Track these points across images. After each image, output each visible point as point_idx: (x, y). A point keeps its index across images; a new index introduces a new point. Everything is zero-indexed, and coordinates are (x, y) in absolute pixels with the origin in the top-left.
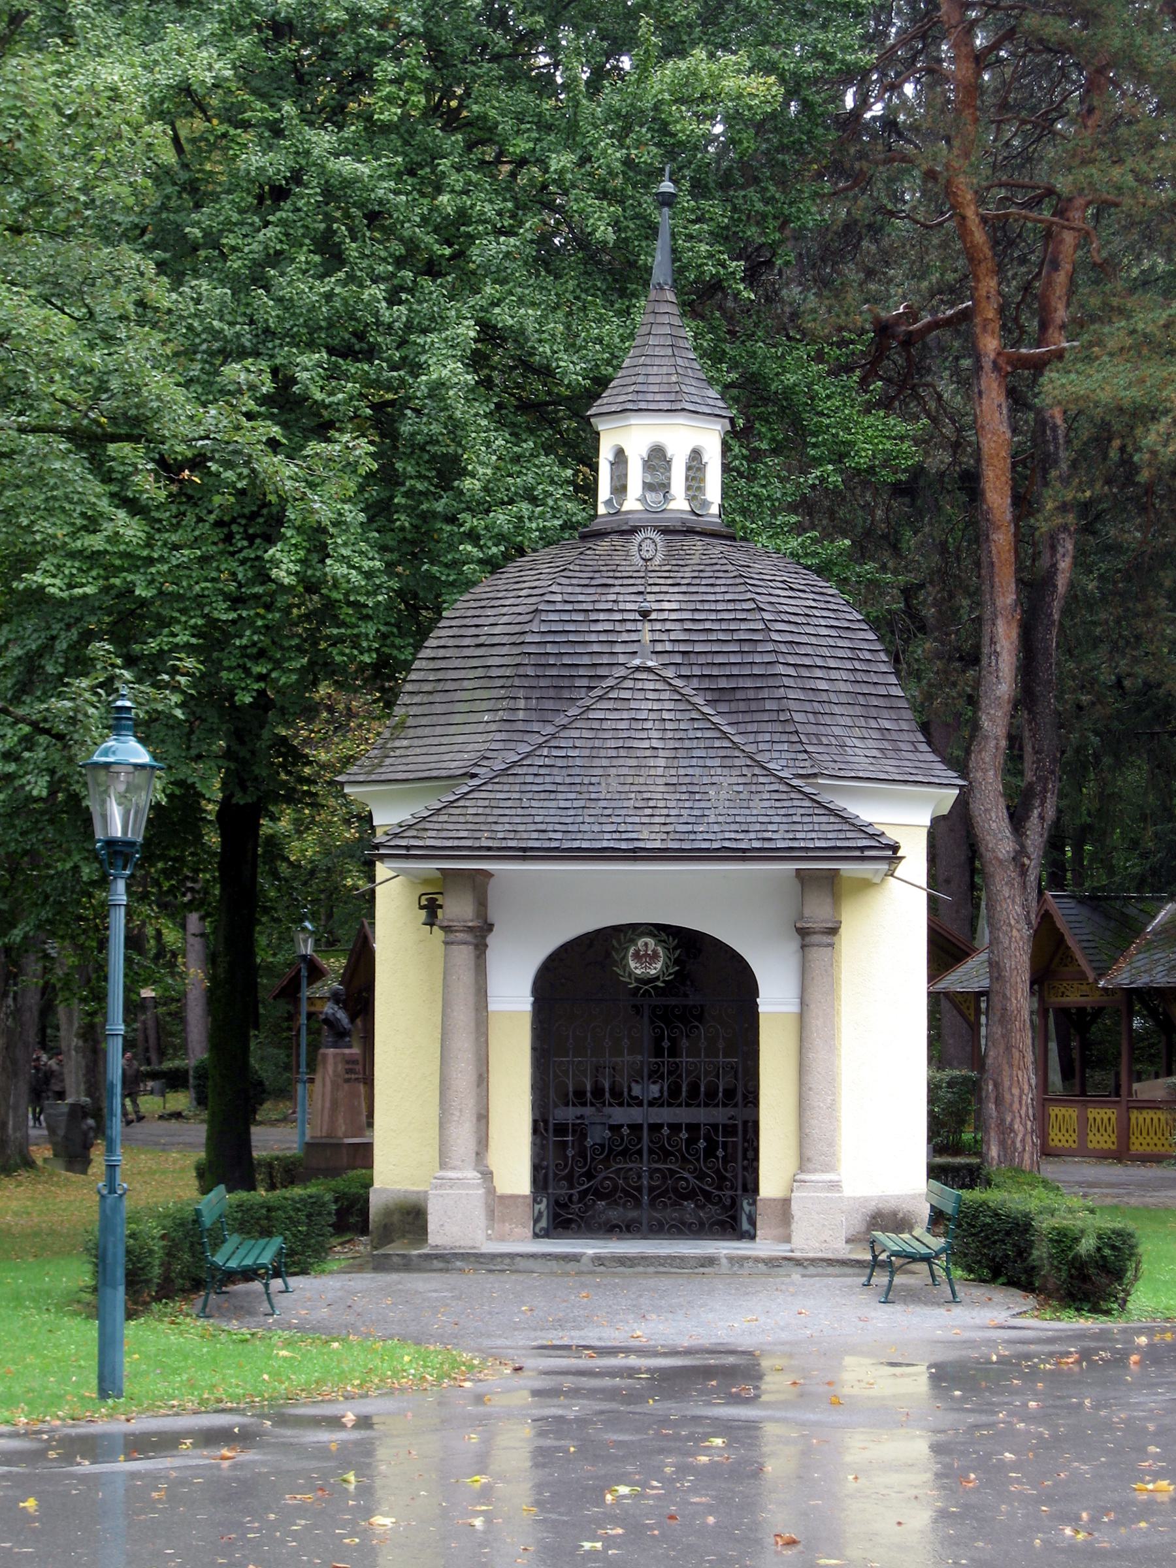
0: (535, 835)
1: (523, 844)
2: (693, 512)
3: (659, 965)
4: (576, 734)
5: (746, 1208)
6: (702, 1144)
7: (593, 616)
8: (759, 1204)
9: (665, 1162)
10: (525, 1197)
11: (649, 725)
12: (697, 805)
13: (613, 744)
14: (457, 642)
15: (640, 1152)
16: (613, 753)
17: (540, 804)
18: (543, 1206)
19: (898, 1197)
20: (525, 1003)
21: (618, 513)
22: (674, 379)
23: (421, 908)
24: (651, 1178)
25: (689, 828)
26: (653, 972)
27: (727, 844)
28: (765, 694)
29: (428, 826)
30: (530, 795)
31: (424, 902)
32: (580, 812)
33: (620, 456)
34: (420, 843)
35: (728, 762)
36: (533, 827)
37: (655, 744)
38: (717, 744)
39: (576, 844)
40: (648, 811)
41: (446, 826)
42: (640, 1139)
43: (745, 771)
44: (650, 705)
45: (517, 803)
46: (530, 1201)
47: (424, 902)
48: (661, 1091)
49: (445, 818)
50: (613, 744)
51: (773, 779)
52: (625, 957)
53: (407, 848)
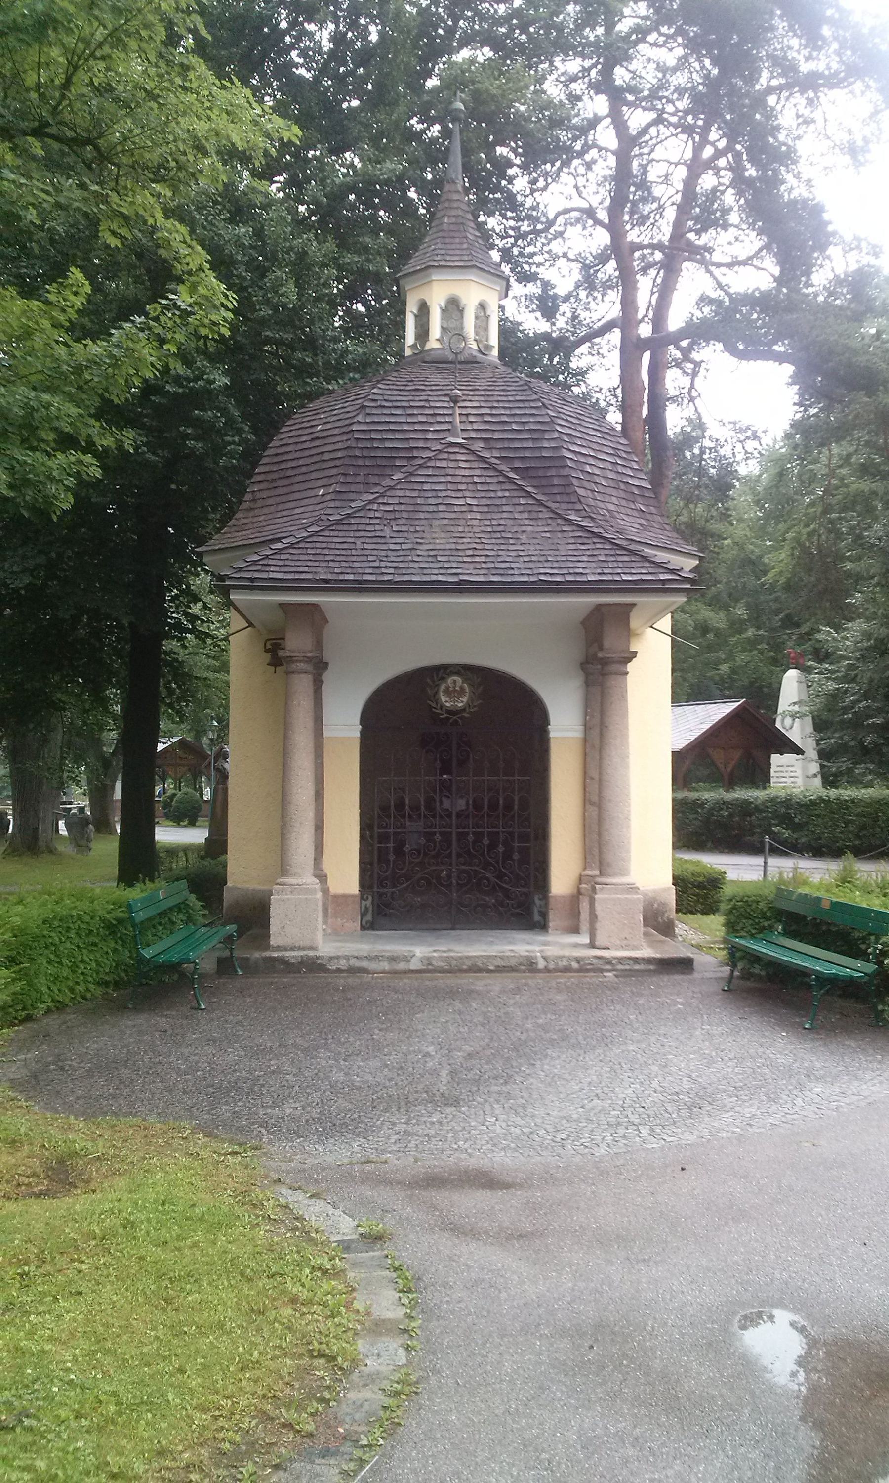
0: (370, 571)
1: (359, 578)
2: (480, 351)
3: (465, 700)
4: (401, 493)
5: (537, 902)
6: (501, 849)
7: (410, 412)
8: (552, 901)
9: (470, 865)
10: (353, 896)
11: (463, 487)
12: (511, 548)
13: (433, 501)
14: (297, 440)
15: (450, 856)
16: (434, 508)
17: (374, 546)
18: (369, 903)
19: (654, 891)
20: (355, 732)
21: (421, 352)
22: (465, 246)
23: (267, 651)
24: (459, 877)
25: (507, 565)
26: (460, 705)
27: (543, 578)
28: (553, 472)
29: (270, 562)
30: (363, 540)
31: (269, 646)
32: (408, 553)
33: (424, 309)
34: (264, 576)
35: (534, 515)
36: (367, 564)
37: (469, 501)
38: (522, 501)
39: (406, 578)
40: (470, 552)
41: (287, 563)
42: (450, 845)
43: (550, 521)
44: (463, 472)
45: (352, 546)
46: (358, 899)
47: (269, 646)
48: (467, 804)
49: (287, 556)
50: (433, 501)
51: (575, 528)
52: (437, 693)
53: (251, 580)
